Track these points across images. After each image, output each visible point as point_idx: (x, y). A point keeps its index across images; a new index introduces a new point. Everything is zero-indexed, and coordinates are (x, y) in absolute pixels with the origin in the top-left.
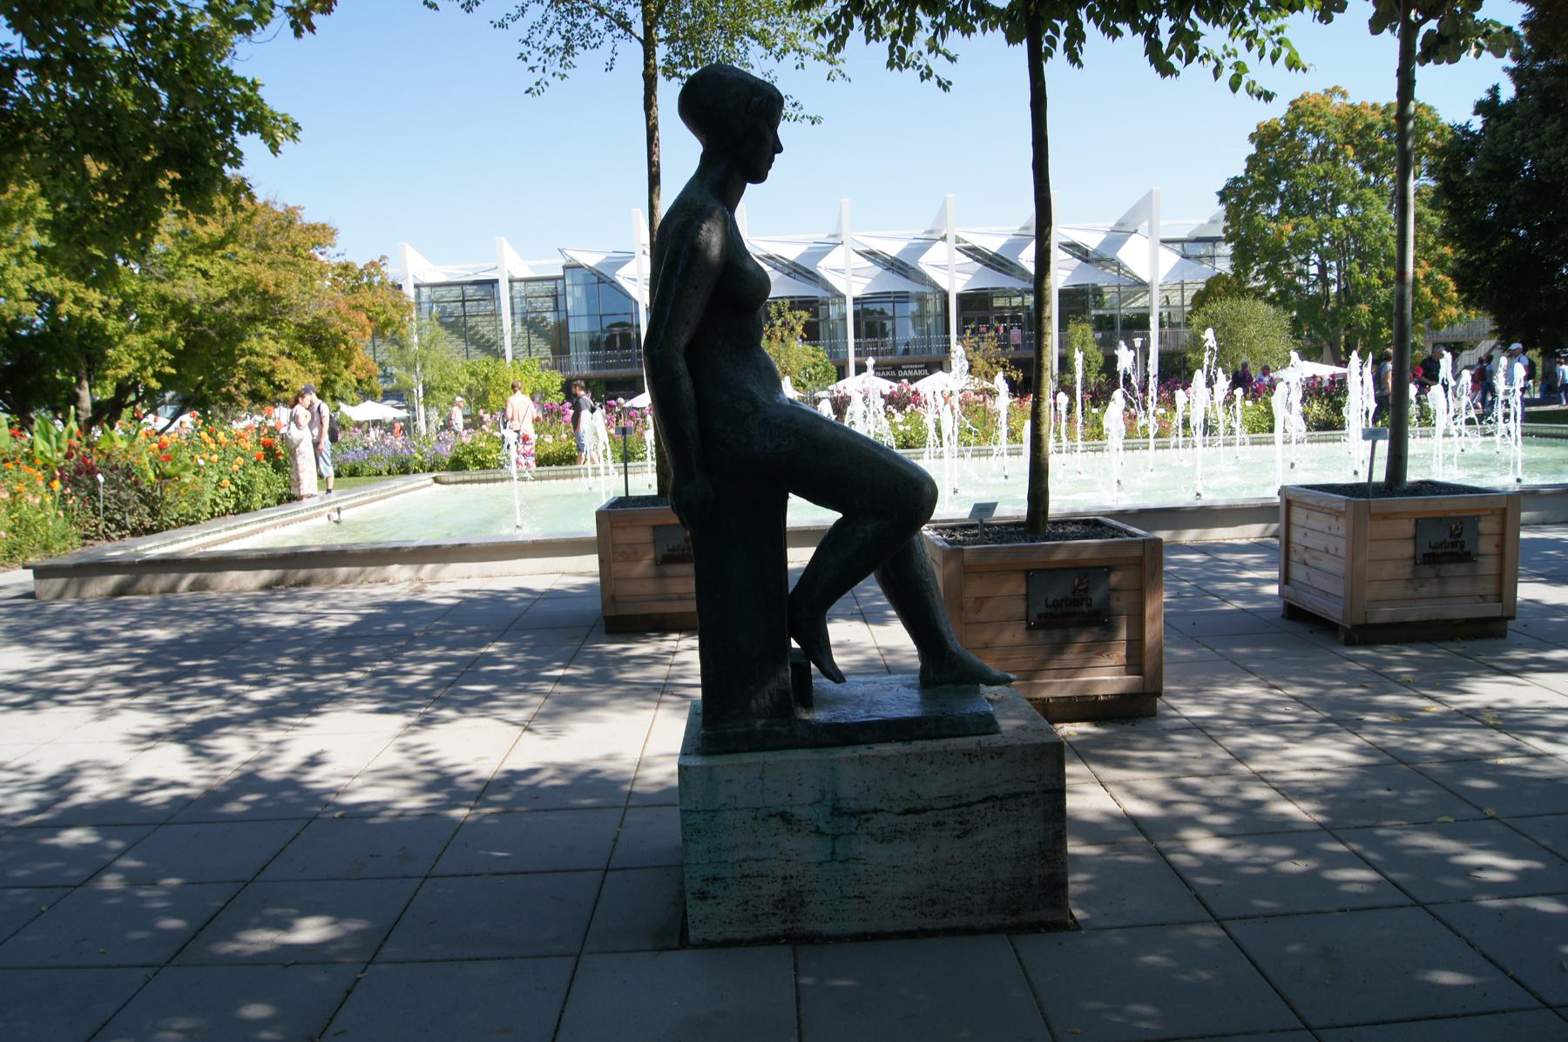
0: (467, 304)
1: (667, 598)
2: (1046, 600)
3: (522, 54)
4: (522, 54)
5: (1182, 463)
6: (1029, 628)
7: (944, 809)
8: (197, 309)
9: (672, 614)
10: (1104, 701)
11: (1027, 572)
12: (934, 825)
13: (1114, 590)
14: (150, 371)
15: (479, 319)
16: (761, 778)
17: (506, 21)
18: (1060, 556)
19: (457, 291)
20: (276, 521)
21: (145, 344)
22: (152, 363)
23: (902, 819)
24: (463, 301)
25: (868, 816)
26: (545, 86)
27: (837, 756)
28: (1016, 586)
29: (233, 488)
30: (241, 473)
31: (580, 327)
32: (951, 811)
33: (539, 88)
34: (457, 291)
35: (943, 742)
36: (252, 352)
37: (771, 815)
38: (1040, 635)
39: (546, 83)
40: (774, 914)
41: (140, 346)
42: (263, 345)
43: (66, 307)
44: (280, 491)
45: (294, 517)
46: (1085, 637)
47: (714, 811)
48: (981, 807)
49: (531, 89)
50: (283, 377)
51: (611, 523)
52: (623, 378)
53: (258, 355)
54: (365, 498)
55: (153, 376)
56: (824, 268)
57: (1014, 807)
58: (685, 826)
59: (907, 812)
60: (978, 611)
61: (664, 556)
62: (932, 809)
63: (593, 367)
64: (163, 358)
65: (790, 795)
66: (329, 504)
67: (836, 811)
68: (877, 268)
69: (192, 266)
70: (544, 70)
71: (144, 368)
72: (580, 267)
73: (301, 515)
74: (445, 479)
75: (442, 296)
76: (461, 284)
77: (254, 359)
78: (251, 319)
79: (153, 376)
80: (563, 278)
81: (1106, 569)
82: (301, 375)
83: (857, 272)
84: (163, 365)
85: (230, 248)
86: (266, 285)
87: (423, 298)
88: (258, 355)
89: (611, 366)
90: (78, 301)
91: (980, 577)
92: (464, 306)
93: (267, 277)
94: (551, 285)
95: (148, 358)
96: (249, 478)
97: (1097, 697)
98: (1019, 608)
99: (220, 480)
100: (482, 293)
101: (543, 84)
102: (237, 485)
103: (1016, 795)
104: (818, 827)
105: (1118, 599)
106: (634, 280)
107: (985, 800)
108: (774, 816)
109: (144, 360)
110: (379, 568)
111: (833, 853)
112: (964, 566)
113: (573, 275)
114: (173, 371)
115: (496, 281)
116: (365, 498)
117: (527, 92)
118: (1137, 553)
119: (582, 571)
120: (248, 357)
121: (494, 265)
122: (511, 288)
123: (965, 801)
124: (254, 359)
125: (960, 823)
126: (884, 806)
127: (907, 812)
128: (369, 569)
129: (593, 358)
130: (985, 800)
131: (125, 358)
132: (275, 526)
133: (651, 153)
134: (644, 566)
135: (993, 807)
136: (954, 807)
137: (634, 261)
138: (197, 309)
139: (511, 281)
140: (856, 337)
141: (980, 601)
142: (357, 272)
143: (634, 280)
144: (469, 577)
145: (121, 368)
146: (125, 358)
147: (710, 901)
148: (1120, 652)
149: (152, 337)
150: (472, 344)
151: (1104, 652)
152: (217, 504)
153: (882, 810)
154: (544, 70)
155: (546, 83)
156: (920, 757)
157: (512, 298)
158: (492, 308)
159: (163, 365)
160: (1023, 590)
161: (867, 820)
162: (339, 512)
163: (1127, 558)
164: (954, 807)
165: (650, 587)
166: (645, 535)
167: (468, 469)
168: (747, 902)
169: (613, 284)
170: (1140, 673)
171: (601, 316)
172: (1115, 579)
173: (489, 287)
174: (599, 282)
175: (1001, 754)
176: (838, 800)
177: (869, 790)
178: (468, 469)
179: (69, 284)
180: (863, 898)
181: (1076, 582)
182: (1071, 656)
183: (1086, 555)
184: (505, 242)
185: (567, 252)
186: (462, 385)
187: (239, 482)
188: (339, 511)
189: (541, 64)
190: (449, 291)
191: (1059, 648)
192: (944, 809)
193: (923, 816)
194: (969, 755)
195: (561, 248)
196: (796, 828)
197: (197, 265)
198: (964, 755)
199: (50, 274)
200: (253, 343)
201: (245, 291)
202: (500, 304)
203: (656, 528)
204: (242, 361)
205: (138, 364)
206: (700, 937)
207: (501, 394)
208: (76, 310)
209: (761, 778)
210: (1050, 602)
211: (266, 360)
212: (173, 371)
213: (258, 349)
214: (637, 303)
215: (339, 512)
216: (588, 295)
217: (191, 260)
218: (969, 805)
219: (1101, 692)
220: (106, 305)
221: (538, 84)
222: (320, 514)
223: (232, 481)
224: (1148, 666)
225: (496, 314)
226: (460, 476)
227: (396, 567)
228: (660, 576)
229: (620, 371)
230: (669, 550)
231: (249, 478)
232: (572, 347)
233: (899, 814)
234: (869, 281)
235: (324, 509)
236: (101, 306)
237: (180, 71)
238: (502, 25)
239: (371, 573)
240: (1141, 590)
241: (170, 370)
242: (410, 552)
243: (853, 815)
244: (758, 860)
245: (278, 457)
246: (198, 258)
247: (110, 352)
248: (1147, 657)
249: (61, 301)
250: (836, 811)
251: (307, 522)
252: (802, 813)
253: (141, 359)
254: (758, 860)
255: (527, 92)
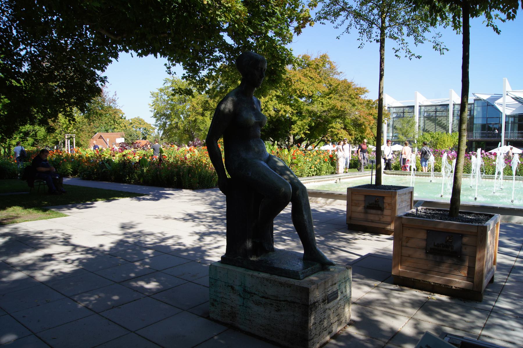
0: (437, 112)
1: (367, 220)
2: (434, 243)
3: (337, 37)
4: (337, 37)
5: (495, 194)
6: (426, 253)
7: (273, 300)
8: (319, 114)
9: (368, 226)
10: (455, 289)
11: (428, 230)
12: (270, 304)
13: (464, 245)
14: (302, 132)
15: (442, 118)
16: (227, 273)
17: (338, 26)
18: (441, 226)
19: (434, 108)
20: (315, 180)
21: (302, 124)
22: (303, 129)
23: (261, 299)
24: (436, 112)
25: (253, 295)
26: (364, 45)
27: (248, 273)
28: (423, 235)
29: (316, 169)
30: (319, 164)
31: (478, 121)
32: (275, 301)
33: (362, 46)
34: (434, 108)
35: (289, 279)
36: (332, 127)
37: (229, 286)
38: (431, 257)
39: (364, 44)
40: (229, 317)
41: (300, 124)
42: (337, 125)
43: (282, 112)
44: (332, 171)
45: (322, 180)
46: (450, 261)
47: (216, 280)
48: (283, 303)
49: (360, 46)
50: (341, 136)
51: (352, 192)
52: (493, 141)
53: (334, 128)
54: (353, 176)
55: (303, 133)
56: (497, 104)
57: (293, 306)
58: (210, 282)
59: (263, 297)
60: (407, 242)
61: (367, 206)
62: (270, 299)
63: (482, 137)
64: (306, 128)
65: (234, 281)
66: (337, 177)
67: (245, 290)
68: (520, 104)
69: (319, 101)
70: (362, 40)
71: (301, 131)
72: (481, 100)
73: (326, 179)
74: (388, 173)
75: (429, 110)
76: (436, 106)
77: (333, 130)
78: (334, 118)
79: (303, 133)
80: (474, 104)
81: (462, 236)
82: (347, 135)
83: (507, 106)
84: (306, 130)
85: (331, 95)
86: (337, 107)
87: (422, 110)
88: (334, 128)
89: (489, 137)
90: (285, 111)
91: (409, 229)
92: (436, 113)
93: (339, 104)
94: (402, 110)
95: (302, 128)
96: (321, 166)
97: (452, 287)
98: (423, 244)
99: (311, 166)
100: (443, 109)
101: (363, 44)
102: (317, 168)
103: (294, 302)
104: (240, 293)
105: (465, 249)
106: (502, 105)
107: (284, 301)
108: (230, 286)
109: (301, 129)
110: (316, 198)
111: (243, 303)
112: (402, 224)
113: (477, 103)
114: (309, 132)
115: (448, 105)
116: (353, 176)
117: (359, 48)
118: (475, 230)
119: (341, 206)
120: (331, 129)
121: (448, 99)
122: (454, 108)
123: (279, 299)
124: (333, 130)
125: (277, 306)
126: (257, 293)
127: (263, 297)
128: (313, 198)
129: (482, 133)
130: (284, 301)
131: (296, 128)
132: (315, 182)
133: (381, 66)
134: (361, 208)
135: (287, 304)
136: (276, 300)
137: (502, 98)
138: (319, 114)
139: (454, 105)
140: (505, 130)
141: (408, 238)
142: (372, 102)
143: (502, 105)
144: (341, 205)
145: (294, 131)
146: (296, 128)
147: (214, 307)
148: (464, 273)
149: (304, 122)
150: (438, 125)
151: (458, 269)
152: (310, 173)
153: (256, 294)
154: (362, 40)
155: (364, 44)
156: (267, 280)
157: (454, 111)
158: (446, 114)
159: (306, 130)
160: (425, 237)
161: (253, 296)
162: (340, 180)
163: (471, 232)
164: (276, 300)
165: (362, 216)
166: (362, 198)
167: (399, 170)
168: (222, 311)
169: (493, 106)
170: (473, 282)
171: (487, 118)
172: (465, 240)
173: (446, 107)
174: (488, 105)
175: (290, 287)
176: (245, 287)
177: (253, 286)
178: (399, 170)
179: (283, 106)
180: (250, 321)
181: (448, 238)
182: (444, 268)
183: (451, 228)
184: (453, 91)
185: (476, 94)
186: (428, 141)
187: (318, 167)
188: (340, 179)
189: (361, 38)
190: (400, 109)
191: (439, 263)
192: (273, 300)
193: (267, 300)
194: (281, 283)
195: (473, 93)
196: (235, 292)
197: (321, 100)
198: (279, 283)
199: (279, 103)
200: (334, 125)
201: (332, 109)
202: (449, 114)
203: (366, 196)
204: (329, 130)
205: (299, 130)
206: (212, 317)
207: (442, 145)
208: (284, 114)
209: (227, 273)
210: (436, 244)
211: (336, 130)
212: (309, 132)
213: (335, 127)
214: (502, 113)
215: (340, 180)
216: (483, 110)
217: (319, 99)
218: (280, 301)
219: (454, 286)
220: (292, 112)
221: (361, 44)
222: (333, 180)
223: (315, 167)
224: (476, 279)
225: (447, 117)
226: (397, 172)
227: (320, 198)
228: (366, 213)
229: (492, 139)
230: (369, 204)
231: (321, 166)
232: (474, 129)
233: (261, 297)
234: (514, 109)
235: (335, 178)
236: (291, 112)
237: (264, 48)
238: (337, 28)
239: (313, 199)
240: (476, 246)
241: (307, 132)
242: (325, 194)
243: (249, 293)
244: (225, 299)
245: (333, 161)
246: (321, 98)
247: (293, 126)
248: (476, 276)
249: (280, 111)
250: (245, 290)
251: (327, 181)
252: (237, 288)
253: (300, 128)
254: (225, 299)
255: (359, 48)
